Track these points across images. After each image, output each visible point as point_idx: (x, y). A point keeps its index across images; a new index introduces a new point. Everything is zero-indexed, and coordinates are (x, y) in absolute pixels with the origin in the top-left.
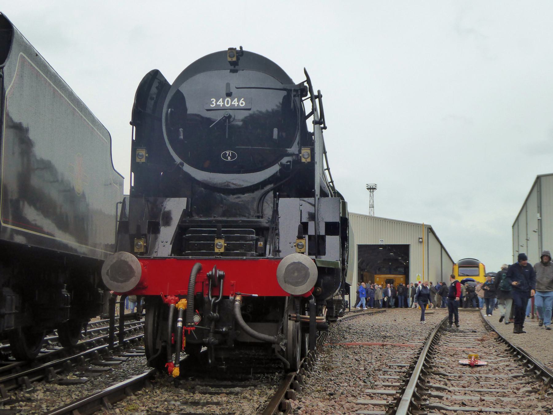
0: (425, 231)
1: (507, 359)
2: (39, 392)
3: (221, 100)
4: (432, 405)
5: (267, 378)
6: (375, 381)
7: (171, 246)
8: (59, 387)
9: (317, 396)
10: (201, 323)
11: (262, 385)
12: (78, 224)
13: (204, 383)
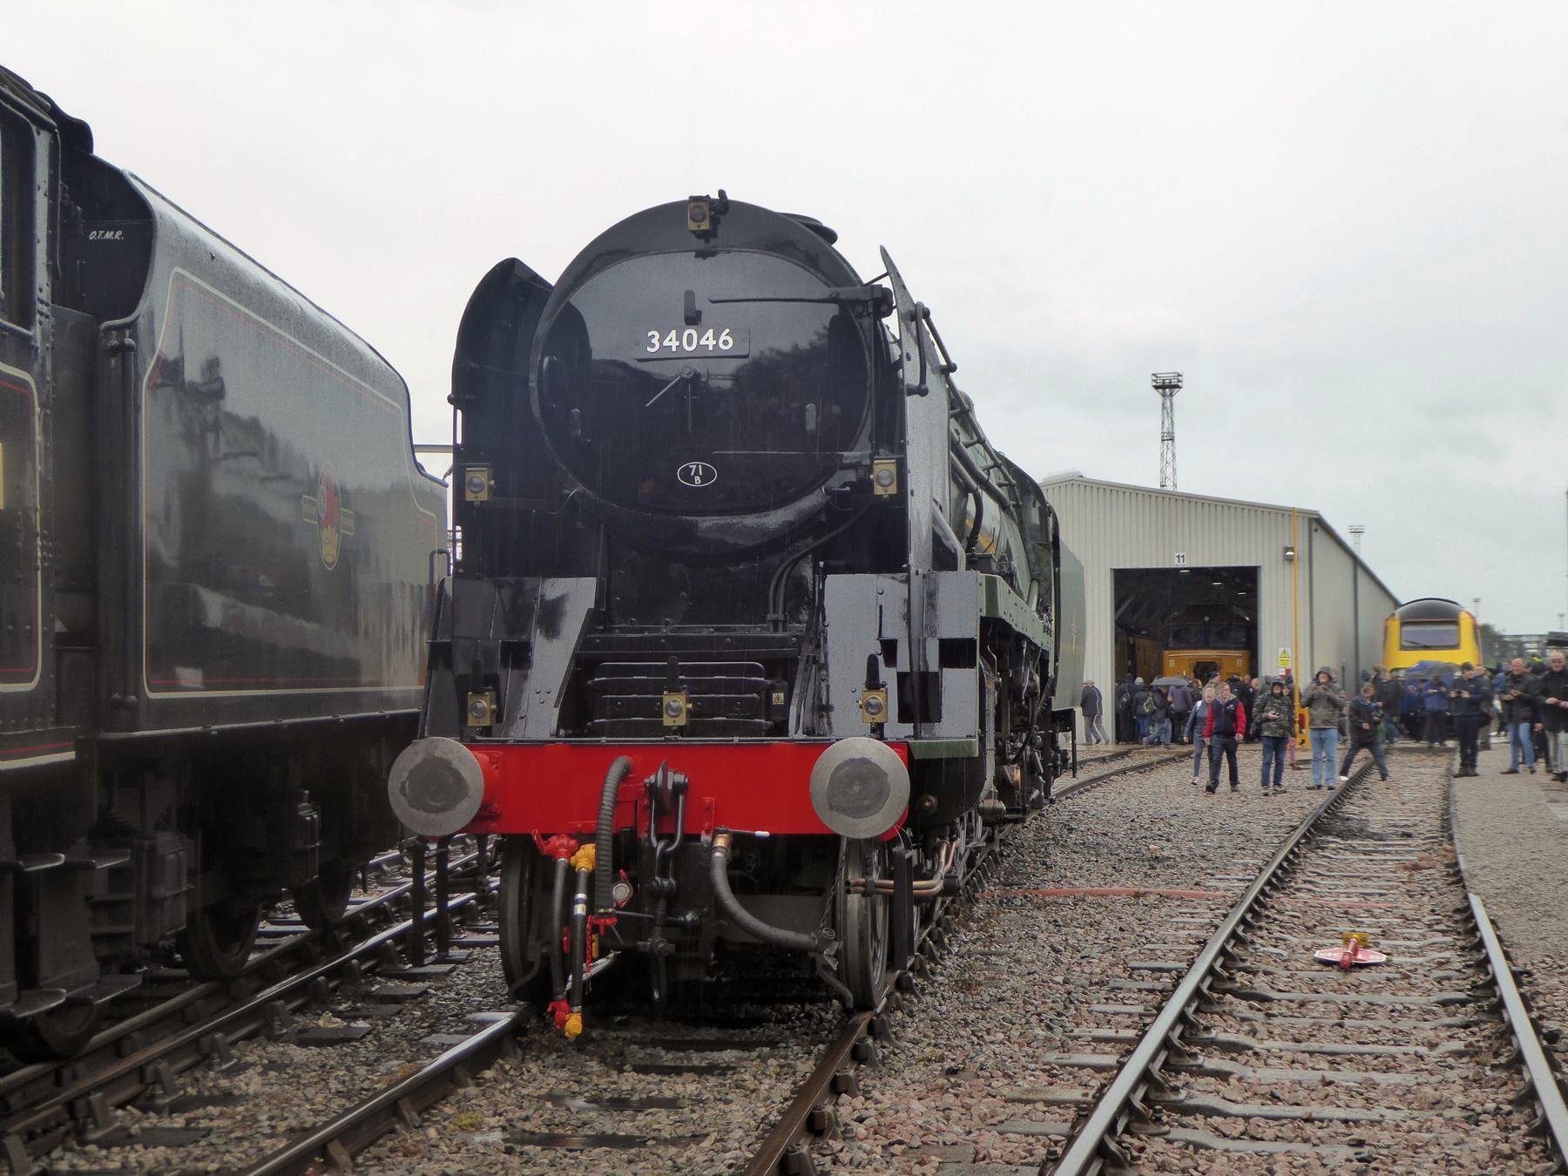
0: (1302, 527)
1: (1449, 939)
2: (250, 1072)
3: (673, 334)
4: (1192, 1102)
5: (809, 1016)
6: (1077, 1025)
7: (557, 711)
8: (298, 1054)
9: (917, 1076)
10: (633, 903)
11: (792, 1042)
12: (343, 592)
13: (650, 1036)
